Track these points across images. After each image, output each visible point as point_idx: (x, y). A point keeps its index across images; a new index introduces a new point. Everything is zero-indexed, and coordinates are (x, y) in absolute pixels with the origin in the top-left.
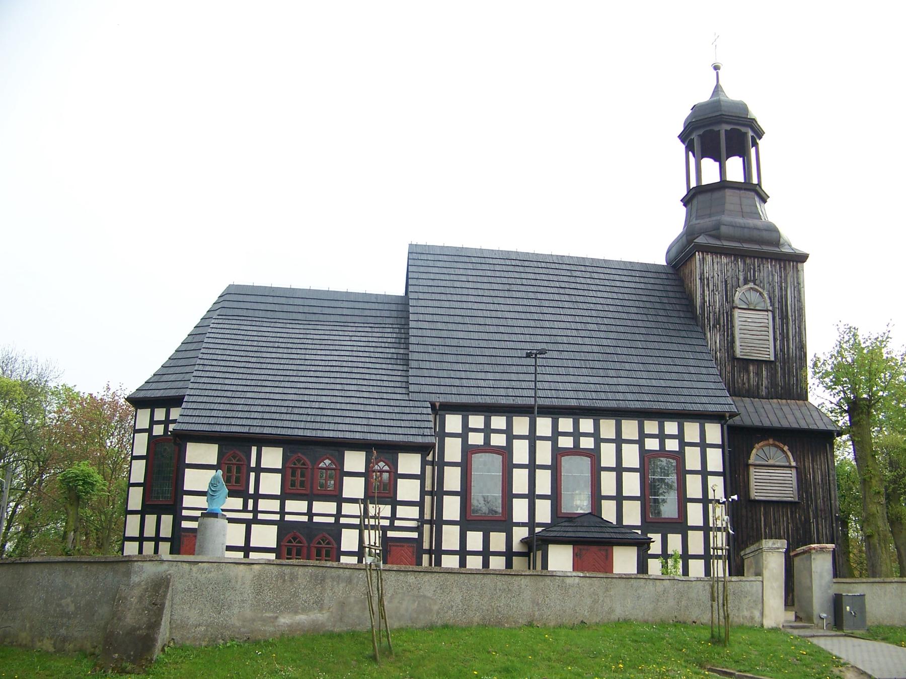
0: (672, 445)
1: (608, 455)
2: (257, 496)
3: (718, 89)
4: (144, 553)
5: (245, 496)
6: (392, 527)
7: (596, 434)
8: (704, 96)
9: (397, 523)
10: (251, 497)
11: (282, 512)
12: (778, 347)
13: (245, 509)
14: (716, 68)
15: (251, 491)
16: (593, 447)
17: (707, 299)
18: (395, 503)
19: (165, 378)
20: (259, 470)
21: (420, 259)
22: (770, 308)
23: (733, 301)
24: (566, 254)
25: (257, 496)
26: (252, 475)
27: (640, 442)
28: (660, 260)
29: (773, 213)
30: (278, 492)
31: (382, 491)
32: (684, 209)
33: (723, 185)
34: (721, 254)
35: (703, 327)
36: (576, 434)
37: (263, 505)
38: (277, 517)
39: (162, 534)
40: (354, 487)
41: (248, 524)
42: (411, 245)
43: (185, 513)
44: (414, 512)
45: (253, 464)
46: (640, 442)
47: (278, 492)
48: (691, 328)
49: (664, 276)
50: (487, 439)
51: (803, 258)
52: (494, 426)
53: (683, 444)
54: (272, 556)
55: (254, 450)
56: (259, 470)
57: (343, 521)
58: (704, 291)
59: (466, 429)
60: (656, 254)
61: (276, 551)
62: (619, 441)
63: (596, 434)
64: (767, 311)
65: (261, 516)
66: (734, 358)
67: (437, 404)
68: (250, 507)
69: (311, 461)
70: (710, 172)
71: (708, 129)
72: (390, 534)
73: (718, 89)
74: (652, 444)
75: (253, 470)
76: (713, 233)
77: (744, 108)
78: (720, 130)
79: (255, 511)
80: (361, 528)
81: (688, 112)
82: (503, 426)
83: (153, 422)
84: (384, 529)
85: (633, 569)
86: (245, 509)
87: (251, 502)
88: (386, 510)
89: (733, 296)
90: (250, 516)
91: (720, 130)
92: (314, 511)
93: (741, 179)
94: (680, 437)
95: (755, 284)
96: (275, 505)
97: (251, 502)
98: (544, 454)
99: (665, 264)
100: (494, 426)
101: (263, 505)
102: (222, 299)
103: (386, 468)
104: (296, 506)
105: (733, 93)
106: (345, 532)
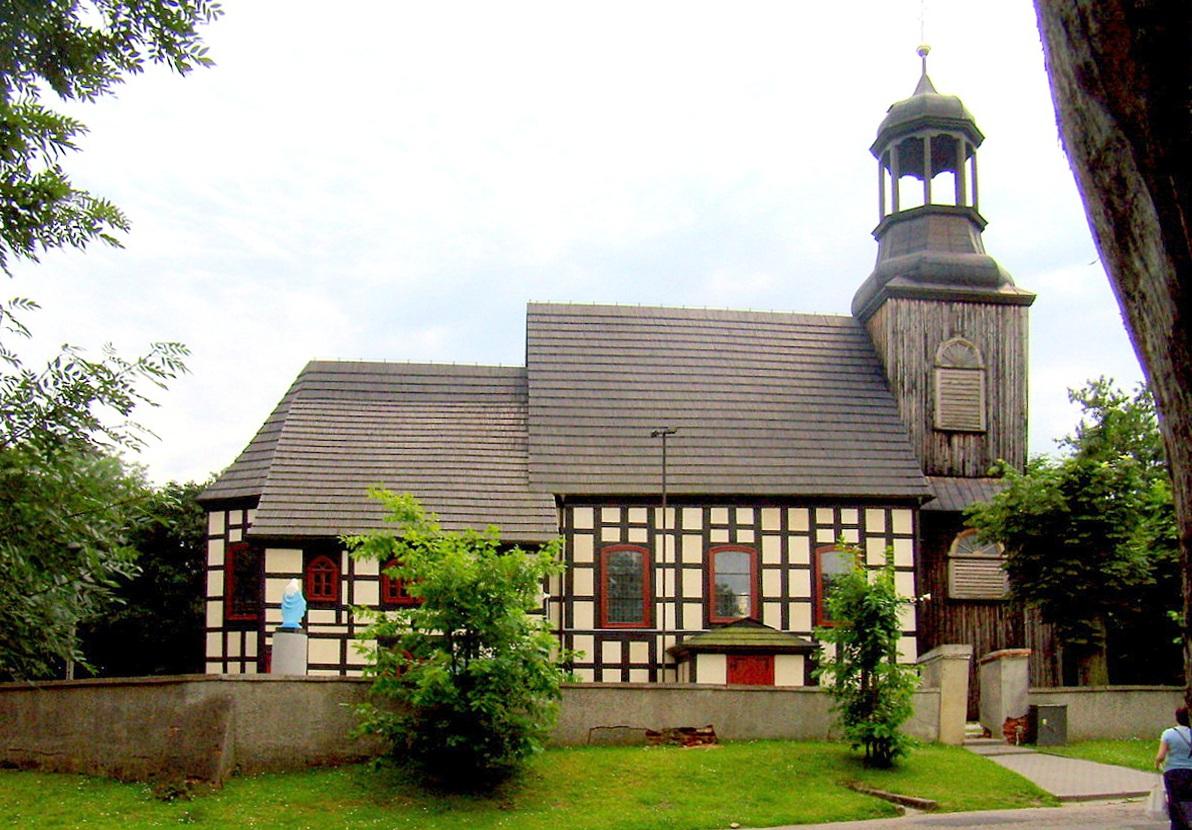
0: (638, 536)
3: (925, 82)
7: (756, 527)
8: (904, 92)
13: (338, 623)
14: (923, 53)
15: (345, 602)
17: (900, 358)
20: (352, 578)
21: (542, 321)
23: (934, 359)
26: (345, 584)
28: (846, 312)
32: (876, 244)
39: (248, 654)
41: (344, 638)
51: (1026, 301)
56: (352, 578)
59: (599, 524)
62: (785, 533)
63: (756, 527)
64: (978, 369)
66: (935, 430)
70: (911, 193)
73: (925, 82)
74: (611, 535)
76: (912, 273)
79: (351, 624)
82: (644, 520)
83: (228, 527)
86: (338, 623)
90: (345, 630)
97: (345, 614)
105: (945, 88)
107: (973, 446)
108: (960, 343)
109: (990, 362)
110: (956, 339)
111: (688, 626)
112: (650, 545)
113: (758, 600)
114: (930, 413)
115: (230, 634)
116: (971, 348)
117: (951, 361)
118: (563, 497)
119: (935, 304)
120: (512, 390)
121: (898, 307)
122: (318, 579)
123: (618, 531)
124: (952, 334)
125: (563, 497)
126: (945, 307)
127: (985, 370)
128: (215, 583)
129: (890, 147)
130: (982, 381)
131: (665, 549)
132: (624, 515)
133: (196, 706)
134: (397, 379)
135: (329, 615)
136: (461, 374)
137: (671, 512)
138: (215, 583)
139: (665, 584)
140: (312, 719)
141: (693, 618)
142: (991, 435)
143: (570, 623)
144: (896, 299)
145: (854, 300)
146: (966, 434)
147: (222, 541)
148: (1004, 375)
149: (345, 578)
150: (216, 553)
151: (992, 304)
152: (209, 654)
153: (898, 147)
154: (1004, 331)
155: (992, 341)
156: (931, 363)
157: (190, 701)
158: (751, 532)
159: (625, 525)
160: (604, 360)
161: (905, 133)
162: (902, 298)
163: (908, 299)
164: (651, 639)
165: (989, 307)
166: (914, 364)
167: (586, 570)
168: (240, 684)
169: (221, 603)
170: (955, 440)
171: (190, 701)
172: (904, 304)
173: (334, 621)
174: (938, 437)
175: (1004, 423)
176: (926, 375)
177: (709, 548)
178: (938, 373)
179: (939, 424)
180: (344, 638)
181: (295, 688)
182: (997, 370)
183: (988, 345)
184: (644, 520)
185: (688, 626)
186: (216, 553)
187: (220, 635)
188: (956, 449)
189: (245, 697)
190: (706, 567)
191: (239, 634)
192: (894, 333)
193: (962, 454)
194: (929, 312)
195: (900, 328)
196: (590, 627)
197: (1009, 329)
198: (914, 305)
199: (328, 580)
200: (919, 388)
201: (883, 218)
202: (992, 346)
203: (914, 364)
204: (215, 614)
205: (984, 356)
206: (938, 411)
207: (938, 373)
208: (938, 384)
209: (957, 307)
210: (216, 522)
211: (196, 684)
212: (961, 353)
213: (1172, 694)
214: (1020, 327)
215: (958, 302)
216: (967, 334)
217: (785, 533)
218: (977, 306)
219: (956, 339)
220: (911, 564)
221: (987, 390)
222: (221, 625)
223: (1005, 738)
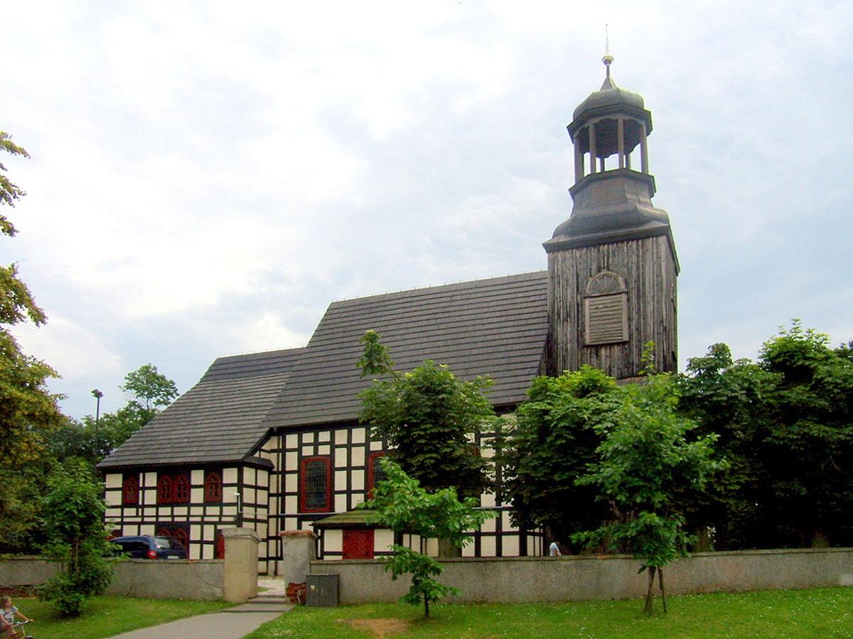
0: (324, 450)
3: (608, 82)
4: (204, 558)
6: (221, 522)
7: (332, 444)
9: (224, 519)
12: (633, 327)
13: (137, 516)
14: (608, 62)
15: (140, 503)
16: (371, 450)
23: (585, 291)
26: (141, 492)
30: (202, 502)
31: (213, 497)
33: (606, 176)
38: (154, 519)
40: (197, 496)
45: (141, 486)
47: (202, 502)
54: (340, 558)
55: (141, 475)
57: (192, 519)
59: (301, 444)
61: (344, 554)
62: (349, 446)
63: (332, 444)
65: (146, 519)
68: (140, 514)
69: (174, 481)
73: (608, 82)
74: (308, 451)
78: (608, 125)
90: (139, 520)
91: (608, 125)
92: (175, 514)
96: (152, 511)
97: (140, 510)
104: (165, 511)
105: (625, 83)
106: (192, 527)
110: (602, 273)
112: (332, 456)
114: (581, 333)
118: (275, 429)
122: (164, 489)
123: (312, 448)
124: (599, 270)
125: (275, 429)
126: (594, 251)
129: (590, 124)
131: (341, 459)
132: (316, 437)
136: (462, 288)
139: (340, 481)
142: (634, 343)
143: (283, 510)
148: (644, 294)
153: (596, 125)
159: (316, 444)
160: (459, 330)
161: (578, 127)
167: (196, 484)
170: (603, 352)
175: (645, 333)
178: (587, 302)
179: (588, 342)
180: (139, 524)
182: (639, 290)
187: (192, 508)
188: (603, 358)
193: (608, 362)
196: (295, 512)
197: (649, 256)
198: (568, 254)
199: (168, 490)
200: (573, 316)
202: (634, 273)
205: (626, 282)
206: (587, 331)
207: (587, 302)
208: (587, 312)
209: (604, 248)
213: (360, 567)
215: (604, 244)
217: (349, 446)
219: (602, 273)
223: (288, 599)
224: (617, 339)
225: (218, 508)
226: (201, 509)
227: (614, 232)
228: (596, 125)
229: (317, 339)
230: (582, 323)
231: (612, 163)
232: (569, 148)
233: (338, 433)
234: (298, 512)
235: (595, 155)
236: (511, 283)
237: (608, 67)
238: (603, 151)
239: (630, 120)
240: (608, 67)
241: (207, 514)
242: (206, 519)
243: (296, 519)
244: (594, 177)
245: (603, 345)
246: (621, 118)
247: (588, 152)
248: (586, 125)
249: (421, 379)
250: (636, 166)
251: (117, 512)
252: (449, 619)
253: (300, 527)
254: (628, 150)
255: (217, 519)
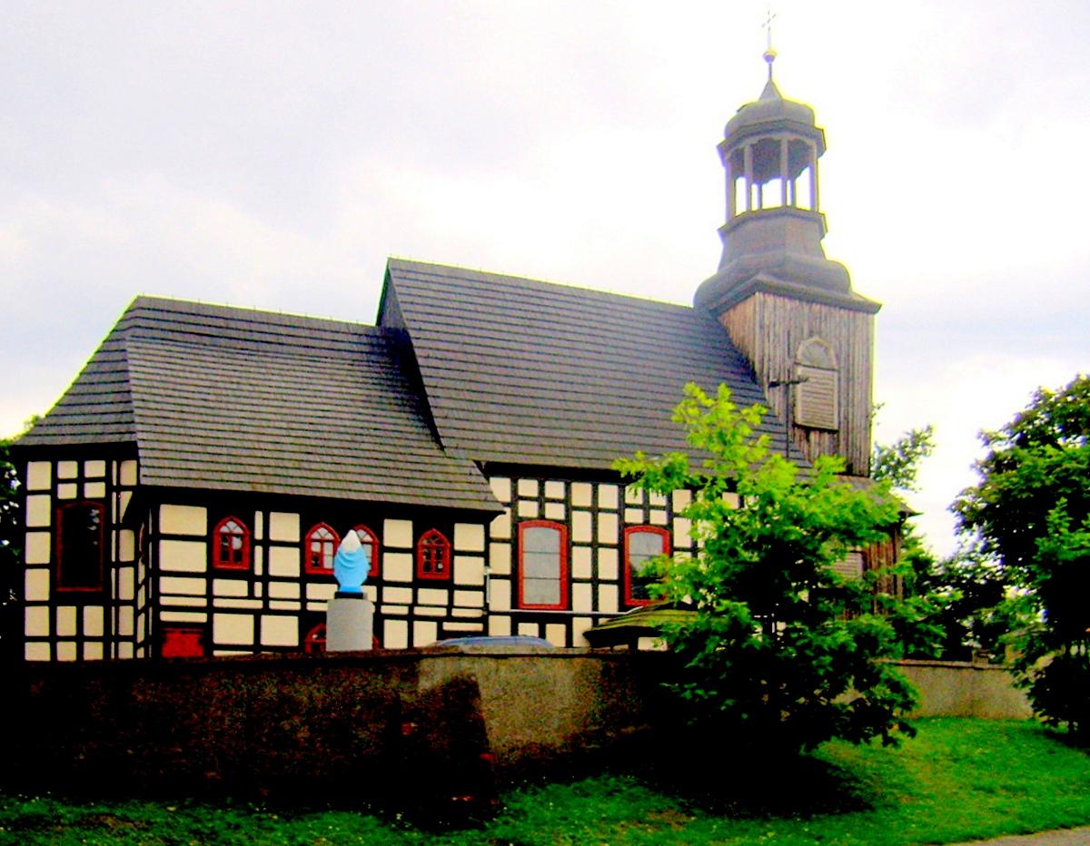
0: (95, 491)
1: (581, 527)
2: (266, 578)
3: (770, 88)
5: (251, 578)
6: (450, 618)
8: (753, 95)
9: (455, 613)
10: (258, 579)
11: (303, 599)
13: (251, 596)
14: (769, 58)
15: (258, 571)
17: (766, 351)
18: (451, 587)
19: (66, 420)
20: (267, 543)
21: (395, 280)
22: (836, 368)
23: (795, 357)
24: (586, 287)
25: (266, 578)
27: (620, 512)
28: (686, 300)
29: (834, 248)
33: (764, 215)
34: (784, 296)
35: (762, 385)
36: (541, 500)
37: (275, 589)
38: (297, 606)
41: (257, 614)
42: (390, 259)
43: (164, 601)
44: (476, 598)
46: (620, 512)
48: (748, 386)
49: (364, 340)
50: (647, 516)
51: (872, 308)
52: (548, 494)
53: (569, 509)
56: (267, 543)
58: (763, 342)
60: (684, 297)
64: (833, 370)
66: (795, 425)
67: (483, 464)
71: (763, 137)
72: (447, 626)
73: (770, 88)
74: (67, 492)
75: (259, 543)
76: (776, 270)
77: (812, 111)
78: (769, 142)
79: (266, 598)
80: (411, 618)
81: (733, 114)
82: (561, 496)
83: (56, 481)
84: (439, 620)
85: (507, 632)
86: (251, 596)
87: (258, 587)
88: (440, 596)
89: (796, 349)
90: (259, 605)
91: (769, 142)
93: (808, 207)
94: (566, 501)
95: (821, 337)
97: (258, 587)
98: (609, 532)
99: (692, 306)
100: (548, 494)
101: (275, 589)
102: (131, 314)
103: (239, 530)
105: (793, 91)
107: (827, 443)
108: (817, 343)
109: (842, 365)
111: (603, 609)
112: (567, 522)
113: (568, 581)
115: (60, 609)
116: (826, 350)
117: (811, 361)
118: (483, 464)
119: (797, 302)
120: (366, 349)
121: (765, 302)
126: (806, 308)
127: (839, 372)
128: (38, 548)
129: (746, 146)
130: (836, 379)
133: (433, 691)
134: (245, 326)
135: (240, 587)
136: (316, 327)
137: (588, 487)
138: (38, 548)
140: (559, 706)
141: (609, 599)
142: (842, 435)
144: (764, 293)
145: (696, 295)
146: (822, 431)
147: (47, 498)
149: (259, 543)
150: (39, 511)
151: (845, 308)
152: (29, 632)
154: (854, 335)
155: (844, 343)
156: (793, 360)
157: (425, 684)
158: (102, 486)
161: (730, 147)
162: (770, 293)
163: (774, 294)
164: (567, 620)
165: (842, 312)
166: (778, 360)
168: (483, 659)
169: (47, 572)
170: (813, 436)
171: (425, 684)
172: (770, 299)
173: (246, 594)
174: (798, 432)
176: (789, 371)
177: (624, 528)
179: (800, 420)
180: (257, 614)
181: (542, 665)
183: (841, 345)
184: (561, 496)
185: (603, 609)
186: (39, 511)
188: (813, 445)
189: (487, 679)
190: (621, 547)
191: (74, 609)
192: (762, 327)
194: (792, 309)
195: (767, 322)
198: (780, 301)
201: (729, 222)
203: (778, 360)
204: (37, 585)
205: (838, 357)
209: (816, 307)
210: (39, 475)
211: (430, 660)
212: (817, 353)
214: (868, 332)
215: (817, 303)
216: (824, 334)
218: (832, 309)
220: (457, 559)
221: (839, 392)
222: (46, 598)
224: (827, 425)
225: (445, 593)
226: (409, 591)
227: (804, 287)
228: (752, 146)
229: (95, 368)
230: (794, 396)
231: (772, 194)
232: (718, 171)
233: (576, 486)
234: (512, 608)
235: (751, 180)
236: (206, 316)
237: (770, 66)
238: (761, 174)
239: (798, 142)
240: (770, 66)
241: (420, 602)
242: (418, 611)
243: (508, 619)
244: (750, 217)
245: (814, 429)
246: (785, 138)
247: (742, 175)
248: (741, 146)
249: (985, 470)
250: (803, 202)
251: (405, 595)
252: (321, 750)
253: (514, 631)
254: (793, 174)
255: (442, 612)
